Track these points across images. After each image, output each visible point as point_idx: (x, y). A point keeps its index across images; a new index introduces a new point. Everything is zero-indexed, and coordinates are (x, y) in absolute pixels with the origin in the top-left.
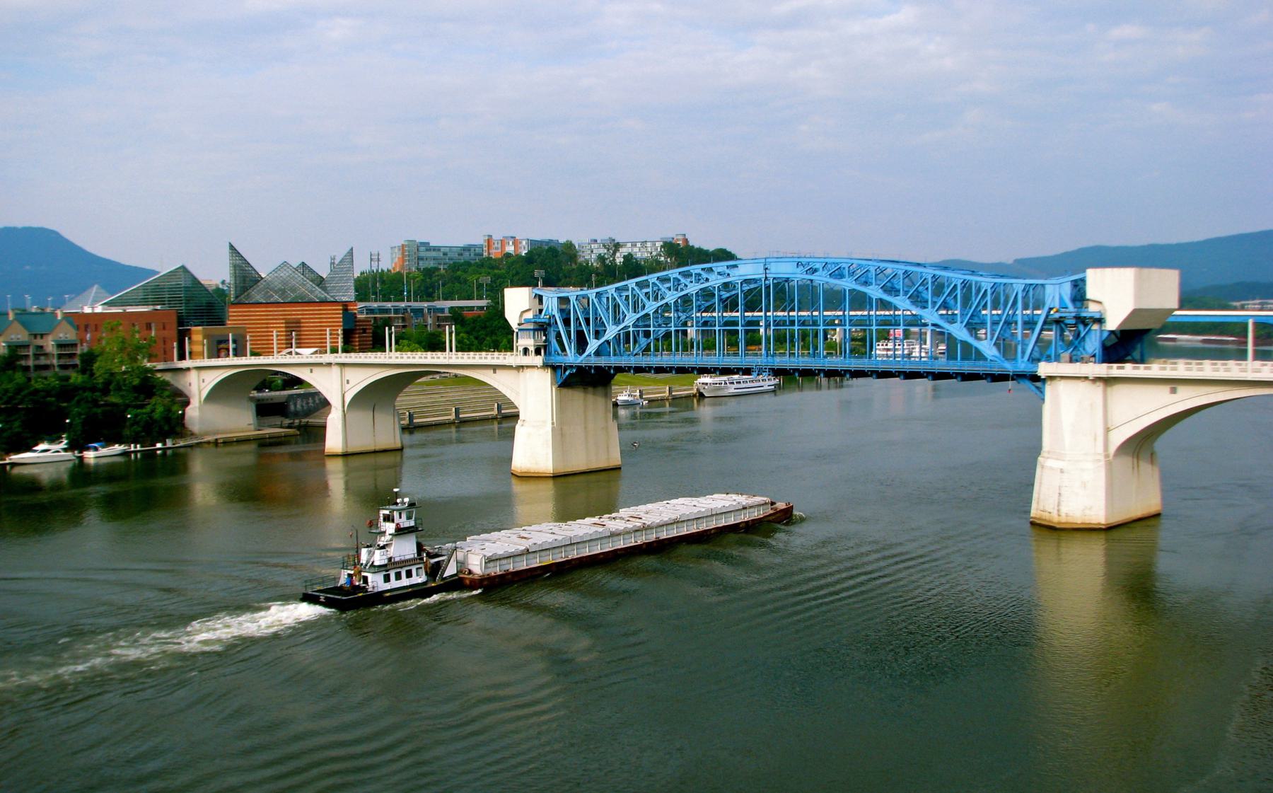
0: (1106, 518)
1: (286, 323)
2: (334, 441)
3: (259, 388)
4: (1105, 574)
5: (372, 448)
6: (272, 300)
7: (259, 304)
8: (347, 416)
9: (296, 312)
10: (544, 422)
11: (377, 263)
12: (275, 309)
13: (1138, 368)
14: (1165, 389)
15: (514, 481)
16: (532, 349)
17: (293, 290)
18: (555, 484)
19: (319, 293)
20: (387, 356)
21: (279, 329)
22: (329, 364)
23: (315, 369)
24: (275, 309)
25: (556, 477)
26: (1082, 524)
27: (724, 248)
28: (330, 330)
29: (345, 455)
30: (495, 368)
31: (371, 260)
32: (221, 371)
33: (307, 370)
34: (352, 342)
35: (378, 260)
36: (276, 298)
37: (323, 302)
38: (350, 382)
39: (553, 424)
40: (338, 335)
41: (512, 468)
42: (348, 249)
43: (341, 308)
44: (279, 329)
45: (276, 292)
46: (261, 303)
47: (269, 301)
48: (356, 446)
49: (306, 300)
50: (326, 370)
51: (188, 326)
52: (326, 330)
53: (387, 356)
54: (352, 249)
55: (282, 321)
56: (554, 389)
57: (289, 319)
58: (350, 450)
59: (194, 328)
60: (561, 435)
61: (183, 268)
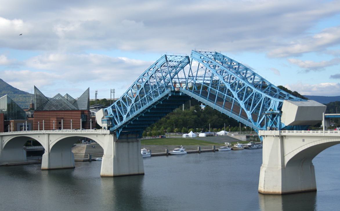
0: (283, 188)
1: (57, 119)
2: (45, 164)
3: (27, 145)
4: (282, 209)
5: (60, 167)
6: (52, 109)
7: (46, 111)
8: (50, 155)
9: (61, 114)
10: (111, 155)
11: (113, 93)
12: (53, 113)
13: (314, 132)
14: (301, 139)
15: (260, 196)
16: (106, 127)
17: (61, 105)
18: (282, 197)
19: (74, 107)
20: (62, 130)
21: (40, 122)
22: (44, 134)
23: (40, 136)
24: (53, 113)
25: (115, 177)
26: (273, 192)
27: (281, 85)
28: (44, 121)
29: (49, 170)
30: (97, 134)
31: (111, 92)
32: (10, 137)
33: (37, 136)
34: (86, 127)
35: (114, 92)
36: (54, 108)
37: (73, 110)
38: (51, 141)
39: (114, 156)
40: (53, 123)
41: (259, 189)
42: (87, 88)
43: (80, 112)
44: (40, 122)
45: (54, 106)
46: (47, 111)
47: (50, 110)
48: (54, 166)
49: (66, 109)
50: (43, 135)
51: (9, 119)
52: (71, 120)
53: (62, 130)
54: (89, 88)
55: (55, 118)
56: (115, 143)
57: (58, 117)
58: (51, 168)
59: (11, 121)
60: (117, 160)
61: (59, 94)
